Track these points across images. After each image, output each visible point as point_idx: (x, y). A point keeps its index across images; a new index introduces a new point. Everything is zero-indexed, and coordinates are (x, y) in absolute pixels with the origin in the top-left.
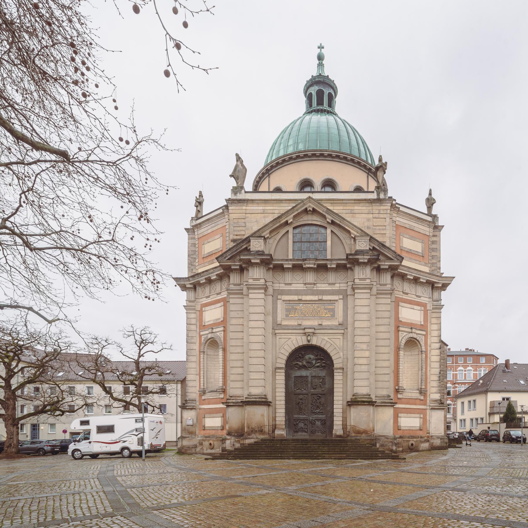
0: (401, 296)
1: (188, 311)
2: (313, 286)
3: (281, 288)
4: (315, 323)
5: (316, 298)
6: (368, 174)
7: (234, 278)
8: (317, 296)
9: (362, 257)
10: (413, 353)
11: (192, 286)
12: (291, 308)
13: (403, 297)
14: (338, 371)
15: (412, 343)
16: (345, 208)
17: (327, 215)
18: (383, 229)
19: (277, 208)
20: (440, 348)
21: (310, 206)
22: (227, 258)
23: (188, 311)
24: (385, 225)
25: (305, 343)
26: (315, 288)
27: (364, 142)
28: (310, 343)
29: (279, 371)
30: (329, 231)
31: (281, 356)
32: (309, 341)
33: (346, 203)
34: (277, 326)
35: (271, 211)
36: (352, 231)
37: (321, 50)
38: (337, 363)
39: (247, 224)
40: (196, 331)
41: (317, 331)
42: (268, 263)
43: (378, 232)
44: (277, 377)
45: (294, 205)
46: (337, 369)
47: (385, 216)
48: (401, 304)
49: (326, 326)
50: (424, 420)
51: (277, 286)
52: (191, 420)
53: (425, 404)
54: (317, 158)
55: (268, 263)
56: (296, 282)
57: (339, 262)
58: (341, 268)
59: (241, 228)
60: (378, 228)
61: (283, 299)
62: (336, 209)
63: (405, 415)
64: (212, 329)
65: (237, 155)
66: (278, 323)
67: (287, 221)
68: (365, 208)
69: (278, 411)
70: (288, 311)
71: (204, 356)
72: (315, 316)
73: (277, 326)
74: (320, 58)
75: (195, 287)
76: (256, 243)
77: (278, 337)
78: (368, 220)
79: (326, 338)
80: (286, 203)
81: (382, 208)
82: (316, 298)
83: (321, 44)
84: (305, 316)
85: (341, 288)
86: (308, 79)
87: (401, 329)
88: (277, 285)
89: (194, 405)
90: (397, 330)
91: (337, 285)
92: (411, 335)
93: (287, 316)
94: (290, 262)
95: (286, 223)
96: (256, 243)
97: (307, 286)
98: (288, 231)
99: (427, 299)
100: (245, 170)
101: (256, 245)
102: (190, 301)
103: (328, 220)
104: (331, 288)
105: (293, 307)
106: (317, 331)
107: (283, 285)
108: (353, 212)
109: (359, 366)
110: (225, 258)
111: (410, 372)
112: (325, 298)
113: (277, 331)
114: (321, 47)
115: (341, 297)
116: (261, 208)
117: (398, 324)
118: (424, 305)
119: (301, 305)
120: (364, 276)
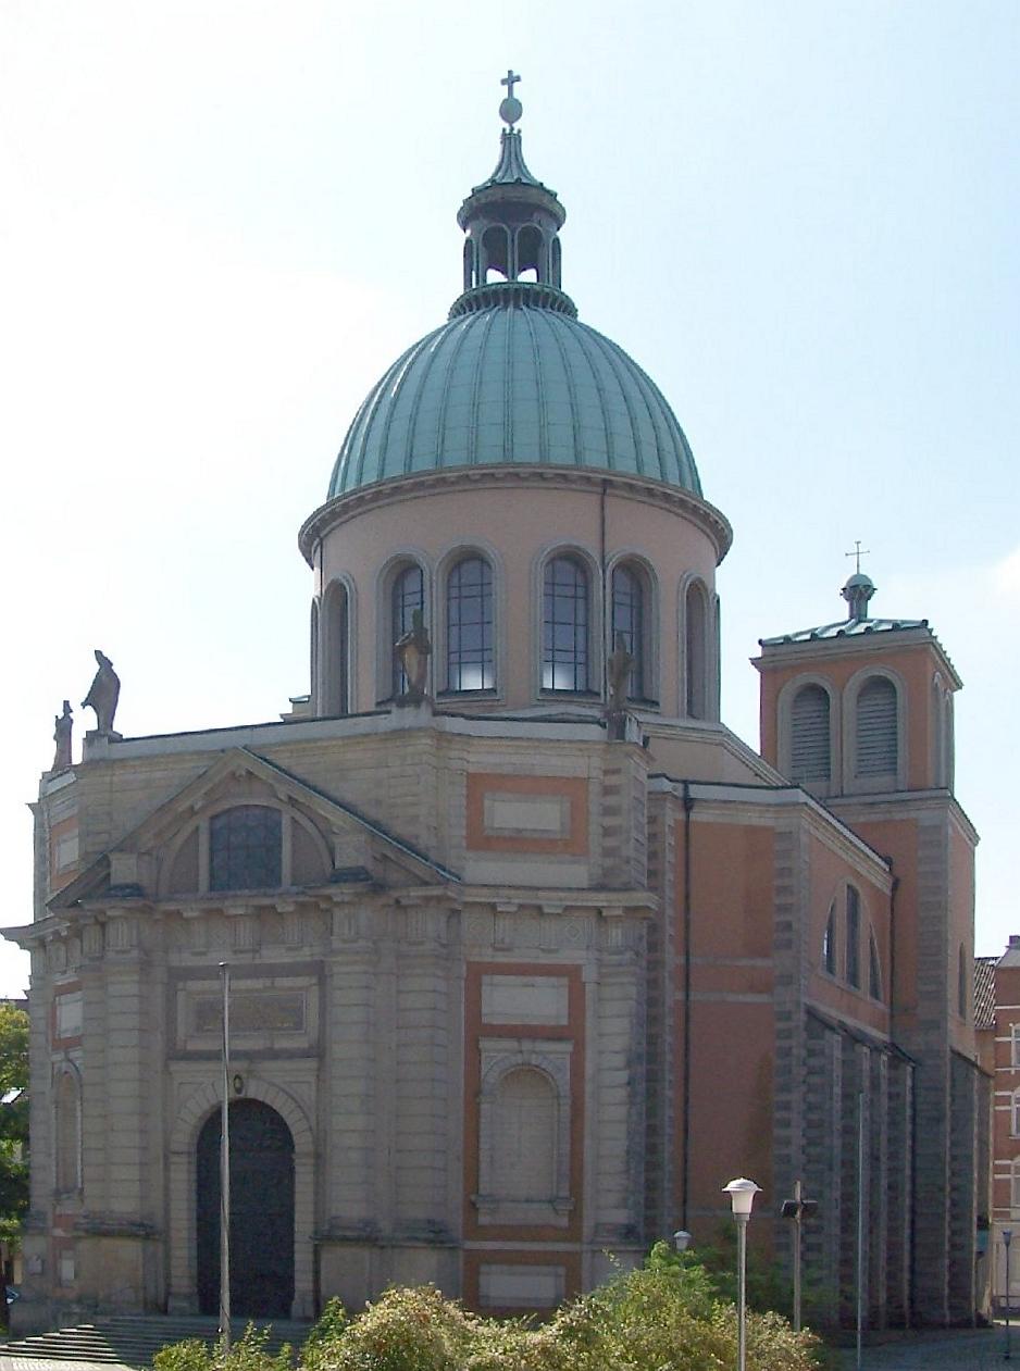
32: (239, 1091)
38: (302, 1142)
51: (175, 960)
67: (192, 808)
74: (511, 110)
91: (306, 950)
95: (192, 812)
117: (478, 1030)
118: (572, 973)
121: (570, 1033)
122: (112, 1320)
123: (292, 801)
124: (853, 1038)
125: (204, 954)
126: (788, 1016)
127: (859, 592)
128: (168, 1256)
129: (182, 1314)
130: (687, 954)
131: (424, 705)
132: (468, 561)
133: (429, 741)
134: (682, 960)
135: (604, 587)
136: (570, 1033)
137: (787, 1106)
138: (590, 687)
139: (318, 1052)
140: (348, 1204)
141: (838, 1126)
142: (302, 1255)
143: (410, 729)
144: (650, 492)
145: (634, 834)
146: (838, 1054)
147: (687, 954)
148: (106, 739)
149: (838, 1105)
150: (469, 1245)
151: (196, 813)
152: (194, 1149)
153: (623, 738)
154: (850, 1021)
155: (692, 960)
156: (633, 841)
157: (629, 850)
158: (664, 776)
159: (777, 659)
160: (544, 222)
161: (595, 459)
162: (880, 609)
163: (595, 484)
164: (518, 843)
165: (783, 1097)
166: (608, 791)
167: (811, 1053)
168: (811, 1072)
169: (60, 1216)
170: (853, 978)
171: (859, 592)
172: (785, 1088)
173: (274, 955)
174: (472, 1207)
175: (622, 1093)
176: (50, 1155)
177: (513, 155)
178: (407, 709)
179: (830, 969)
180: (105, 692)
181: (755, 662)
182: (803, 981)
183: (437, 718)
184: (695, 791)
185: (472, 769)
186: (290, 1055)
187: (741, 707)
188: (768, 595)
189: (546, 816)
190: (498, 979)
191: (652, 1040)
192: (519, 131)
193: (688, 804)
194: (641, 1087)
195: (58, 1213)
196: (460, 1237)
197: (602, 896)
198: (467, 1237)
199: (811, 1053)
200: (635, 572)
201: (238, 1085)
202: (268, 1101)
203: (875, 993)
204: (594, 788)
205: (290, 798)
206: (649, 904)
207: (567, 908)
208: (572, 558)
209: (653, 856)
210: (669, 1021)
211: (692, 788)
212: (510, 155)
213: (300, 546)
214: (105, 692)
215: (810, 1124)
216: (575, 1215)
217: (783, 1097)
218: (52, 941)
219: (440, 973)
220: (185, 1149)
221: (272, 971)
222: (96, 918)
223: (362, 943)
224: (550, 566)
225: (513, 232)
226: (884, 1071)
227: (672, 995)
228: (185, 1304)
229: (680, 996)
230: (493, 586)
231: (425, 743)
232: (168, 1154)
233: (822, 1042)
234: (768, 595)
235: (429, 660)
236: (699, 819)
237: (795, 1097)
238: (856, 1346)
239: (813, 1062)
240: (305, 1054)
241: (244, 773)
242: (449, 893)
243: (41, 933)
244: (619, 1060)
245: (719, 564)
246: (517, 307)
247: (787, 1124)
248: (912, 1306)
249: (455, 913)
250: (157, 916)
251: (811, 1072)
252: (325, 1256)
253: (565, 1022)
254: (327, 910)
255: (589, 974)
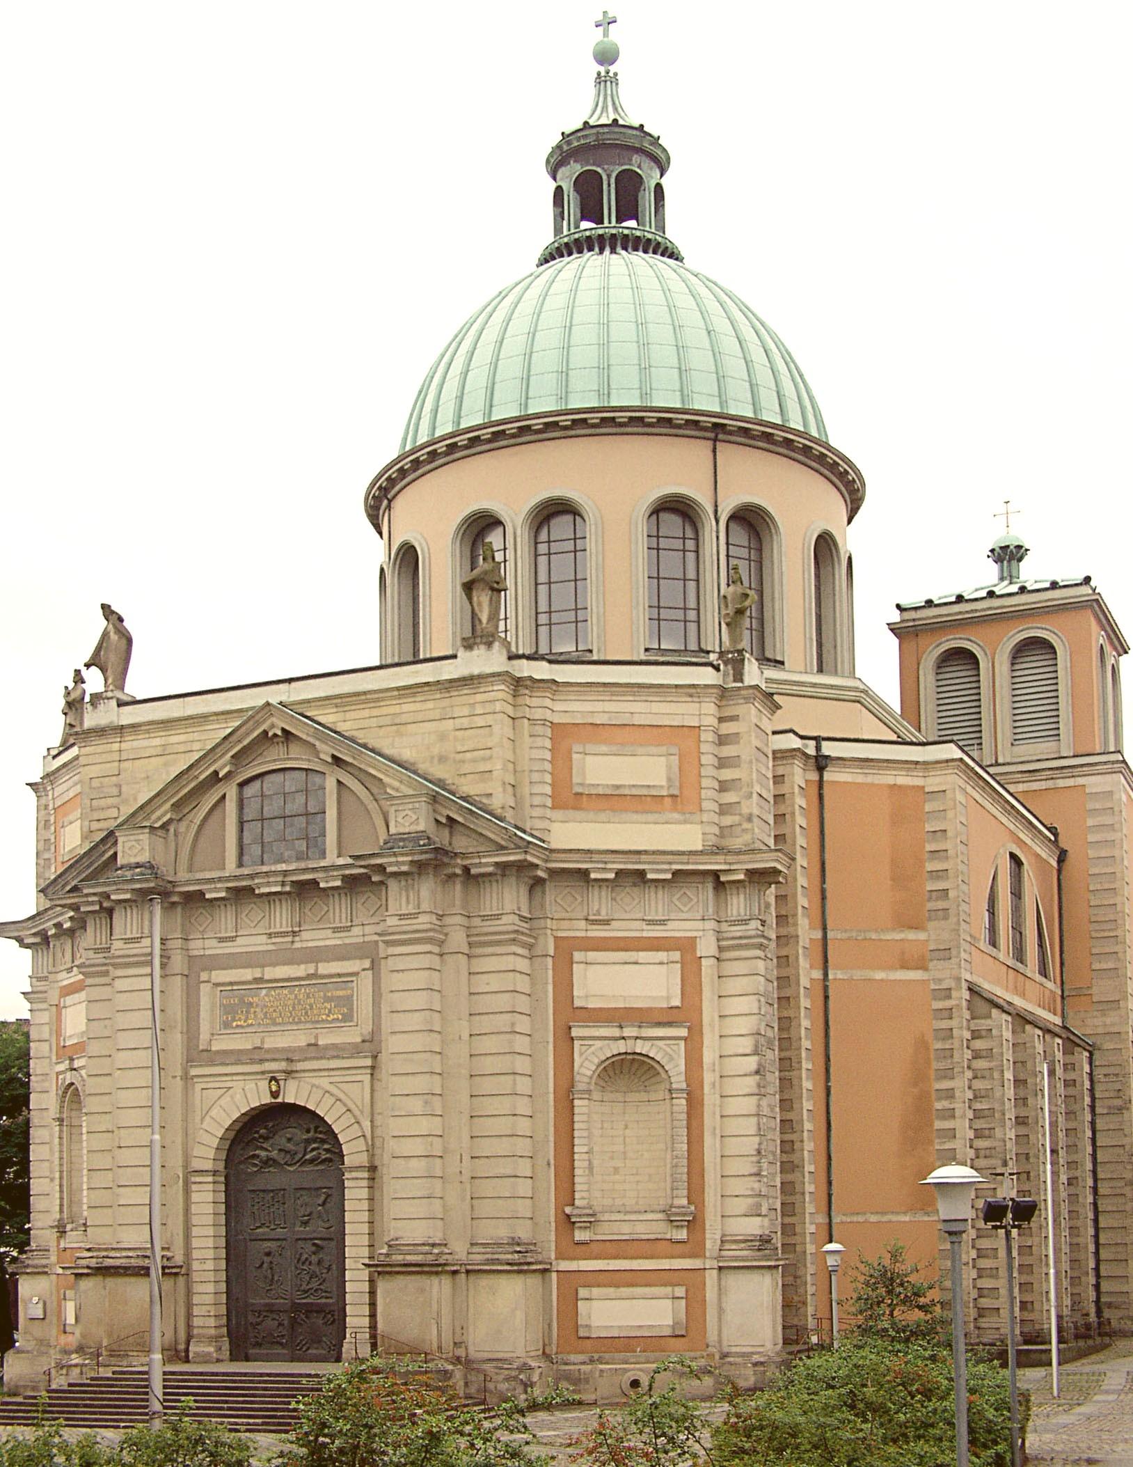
0: (583, 934)
1: (35, 1006)
2: (290, 939)
3: (208, 952)
4: (296, 1039)
5: (300, 971)
6: (715, 440)
7: (91, 937)
8: (303, 966)
9: (393, 859)
10: (653, 1096)
11: (37, 940)
12: (236, 1007)
13: (590, 934)
14: (354, 1174)
15: (631, 1070)
16: (375, 712)
17: (317, 743)
18: (484, 759)
19: (196, 736)
20: (757, 1072)
21: (277, 724)
22: (68, 888)
23: (35, 1006)
24: (489, 745)
25: (267, 1099)
26: (297, 945)
27: (745, 310)
28: (280, 1100)
29: (198, 1179)
30: (331, 784)
31: (206, 1139)
32: (275, 1095)
33: (378, 700)
34: (196, 1055)
35: (182, 748)
36: (386, 780)
37: (606, 34)
38: (353, 1153)
39: (124, 789)
40: (50, 1057)
41: (300, 1066)
42: (158, 892)
43: (467, 768)
44: (195, 1197)
45: (237, 724)
46: (352, 1169)
47: (489, 719)
48: (577, 956)
49: (327, 1047)
50: (695, 1303)
51: (197, 947)
52: (41, 1305)
53: (698, 1253)
54: (512, 441)
55: (158, 892)
56: (252, 933)
57: (347, 872)
58: (353, 884)
59: (110, 801)
60: (468, 755)
61: (213, 981)
62: (347, 722)
63: (611, 1291)
64: (72, 1060)
65: (104, 606)
66: (201, 1047)
67: (216, 773)
68: (430, 705)
69: (197, 1288)
70: (230, 1010)
71: (61, 1131)
72: (300, 1022)
73: (196, 1055)
74: (606, 56)
75: (45, 940)
76: (130, 844)
77: (198, 1087)
78: (442, 737)
79: (324, 1082)
80: (218, 721)
81: (479, 697)
82: (300, 971)
83: (605, 13)
84: (275, 1024)
85: (367, 939)
86: (554, 145)
87: (574, 1033)
88: (199, 943)
89: (44, 1262)
90: (566, 1040)
91: (356, 931)
92: (621, 1047)
93: (227, 1025)
94: (219, 885)
95: (215, 778)
96: (130, 844)
97: (274, 940)
98: (224, 797)
99: (700, 925)
100: (124, 641)
101: (134, 849)
102: (39, 979)
103: (322, 756)
104: (339, 942)
105: (242, 1001)
106: (300, 1066)
107: (214, 943)
108: (397, 721)
109: (402, 1161)
110: (64, 886)
111: (646, 1155)
112: (324, 969)
113: (193, 1072)
114: (607, 22)
115: (367, 963)
116: (157, 742)
117: (570, 1017)
118: (686, 946)
119: (264, 992)
120: (411, 906)
121: (683, 1017)
122: (114, 1373)
123: (337, 761)
124: (1022, 1019)
125: (232, 939)
126: (947, 993)
127: (1008, 556)
128: (189, 1293)
129: (206, 1359)
130: (824, 929)
131: (496, 645)
132: (554, 511)
133: (503, 687)
134: (818, 935)
135: (718, 538)
136: (683, 1017)
137: (950, 1094)
138: (703, 646)
139: (371, 1047)
140: (411, 1219)
141: (1011, 1115)
142: (356, 1280)
143: (480, 677)
144: (768, 437)
145: (757, 788)
146: (1007, 1034)
147: (824, 929)
148: (114, 703)
149: (1010, 1093)
150: (565, 1265)
151: (221, 780)
152: (221, 1166)
153: (742, 681)
154: (1018, 1002)
155: (830, 935)
156: (755, 795)
157: (752, 806)
158: (792, 731)
159: (911, 628)
160: (645, 166)
161: (705, 402)
162: (1032, 572)
163: (705, 429)
164: (616, 801)
165: (946, 1084)
166: (722, 740)
167: (976, 1035)
168: (977, 1055)
169: (65, 1249)
170: (1020, 955)
171: (1008, 556)
172: (948, 1074)
173: (313, 938)
174: (568, 1223)
175: (750, 1083)
176: (52, 1180)
177: (609, 99)
178: (475, 652)
179: (994, 943)
180: (115, 649)
181: (893, 628)
182: (963, 955)
183: (515, 662)
184: (828, 749)
185: (557, 719)
186: (337, 1051)
187: (877, 663)
188: (909, 555)
189: (650, 770)
190: (592, 956)
191: (786, 1023)
192: (616, 74)
193: (821, 763)
194: (774, 1078)
195: (62, 1245)
196: (553, 1257)
197: (721, 858)
198: (560, 1256)
199: (976, 1035)
200: (752, 522)
201: (274, 1088)
202: (311, 1107)
203: (1044, 972)
204: (708, 736)
205: (334, 757)
206: (779, 867)
207: (676, 873)
208: (677, 508)
209: (780, 818)
210: (805, 1002)
211: (824, 744)
212: (605, 98)
213: (366, 511)
214: (115, 649)
215: (978, 1115)
216: (695, 1223)
217: (946, 1084)
218: (54, 935)
219: (520, 951)
220: (209, 1165)
221: (315, 955)
222: (101, 903)
223: (423, 918)
224: (654, 517)
225: (609, 176)
226: (1059, 1055)
227: (807, 974)
228: (212, 1349)
229: (817, 974)
230: (588, 552)
231: (500, 691)
232: (190, 1173)
233: (988, 1022)
234: (909, 555)
235: (599, 876)
236: (831, 779)
237: (960, 1084)
238: (1050, 1364)
239: (978, 1044)
240: (355, 1050)
241: (279, 733)
242: (529, 858)
243: (41, 927)
244: (746, 1045)
245: (849, 522)
246: (613, 251)
247: (951, 1114)
248: (1099, 1312)
249: (539, 882)
250: (175, 899)
251: (977, 1055)
252: (382, 1286)
253: (676, 1002)
254: (382, 883)
255: (706, 947)
